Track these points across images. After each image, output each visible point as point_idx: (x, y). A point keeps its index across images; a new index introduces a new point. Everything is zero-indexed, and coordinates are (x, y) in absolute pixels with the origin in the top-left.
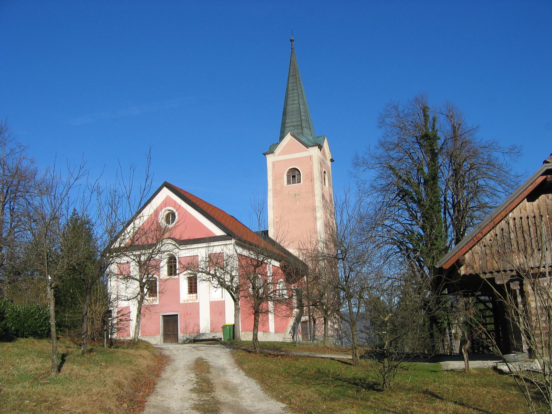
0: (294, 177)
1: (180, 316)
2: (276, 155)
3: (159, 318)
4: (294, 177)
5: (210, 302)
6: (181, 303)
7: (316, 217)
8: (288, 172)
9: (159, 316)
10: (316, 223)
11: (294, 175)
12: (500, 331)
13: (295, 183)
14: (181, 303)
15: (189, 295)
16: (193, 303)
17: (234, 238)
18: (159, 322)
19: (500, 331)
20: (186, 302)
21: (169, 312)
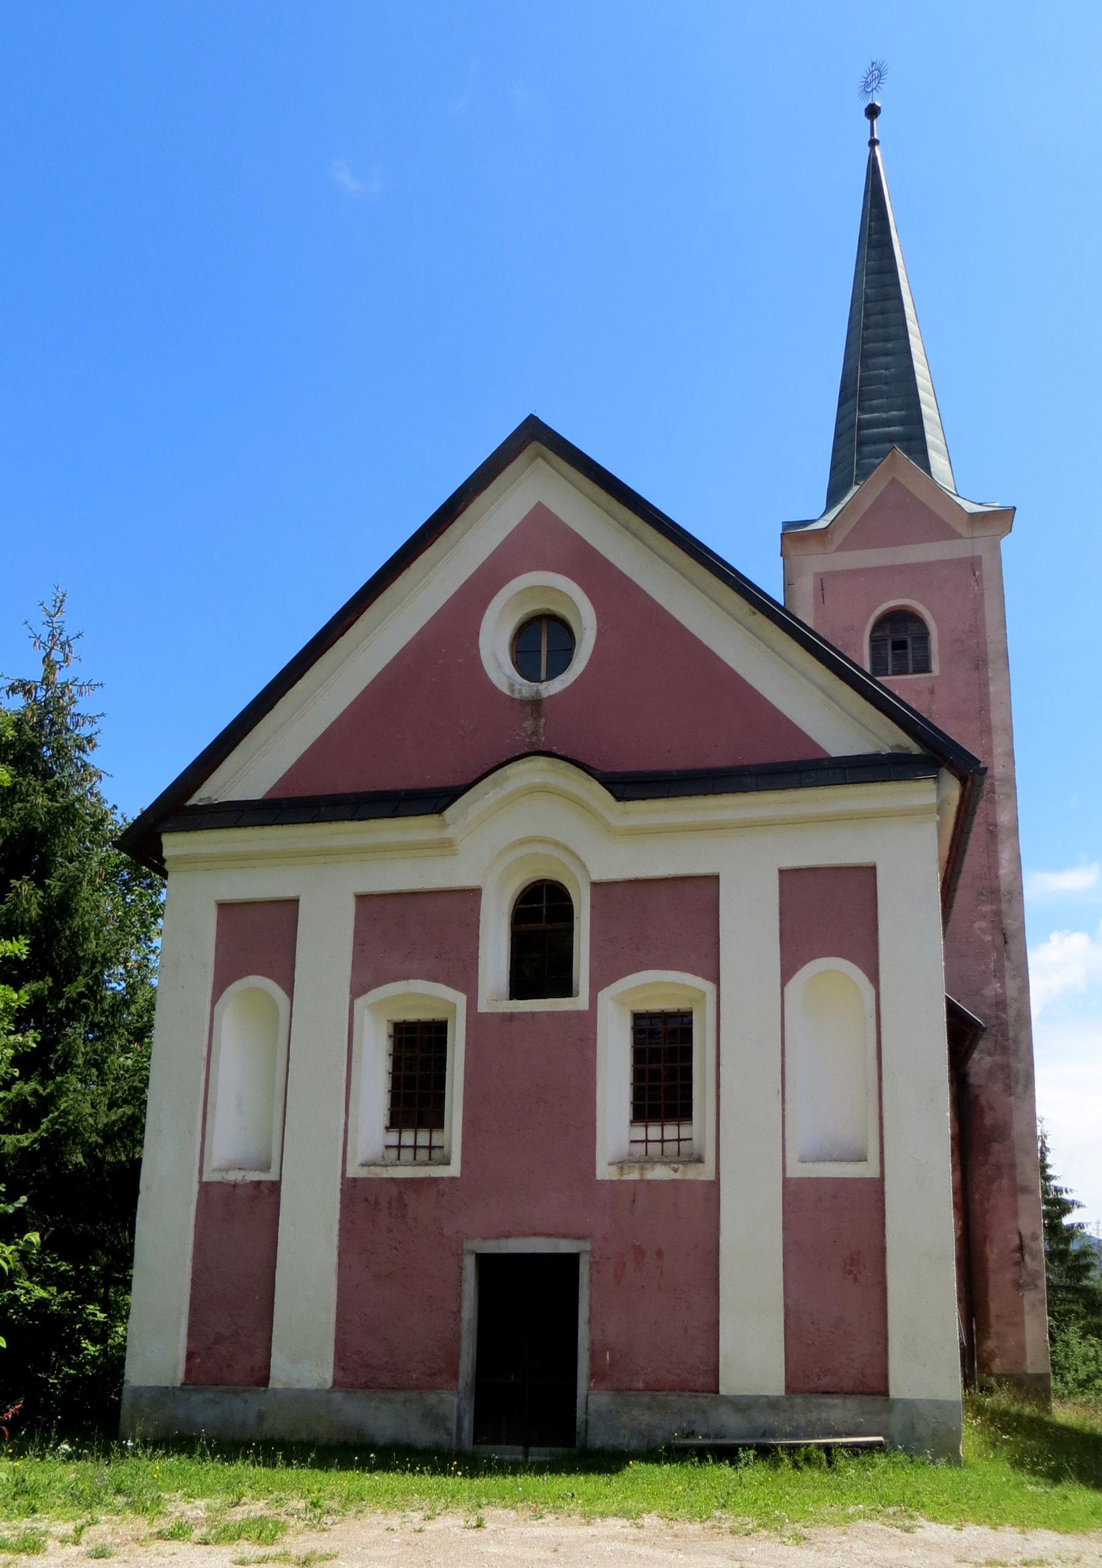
0: (900, 645)
1: (593, 1264)
2: (834, 547)
3: (461, 1268)
4: (900, 645)
5: (205, 1188)
6: (599, 1176)
7: (996, 825)
8: (878, 625)
9: (459, 1256)
10: (995, 852)
11: (899, 637)
12: (34, 1322)
13: (906, 673)
14: (599, 1176)
15: (639, 1133)
16: (674, 1181)
17: (23, 932)
18: (459, 1297)
19: (34, 1322)
20: (635, 1176)
21: (524, 1235)
